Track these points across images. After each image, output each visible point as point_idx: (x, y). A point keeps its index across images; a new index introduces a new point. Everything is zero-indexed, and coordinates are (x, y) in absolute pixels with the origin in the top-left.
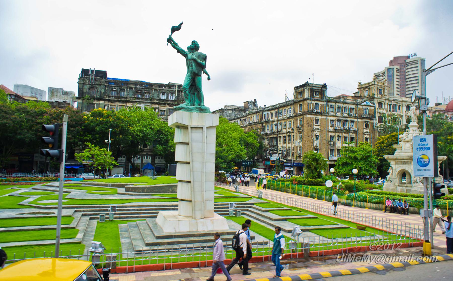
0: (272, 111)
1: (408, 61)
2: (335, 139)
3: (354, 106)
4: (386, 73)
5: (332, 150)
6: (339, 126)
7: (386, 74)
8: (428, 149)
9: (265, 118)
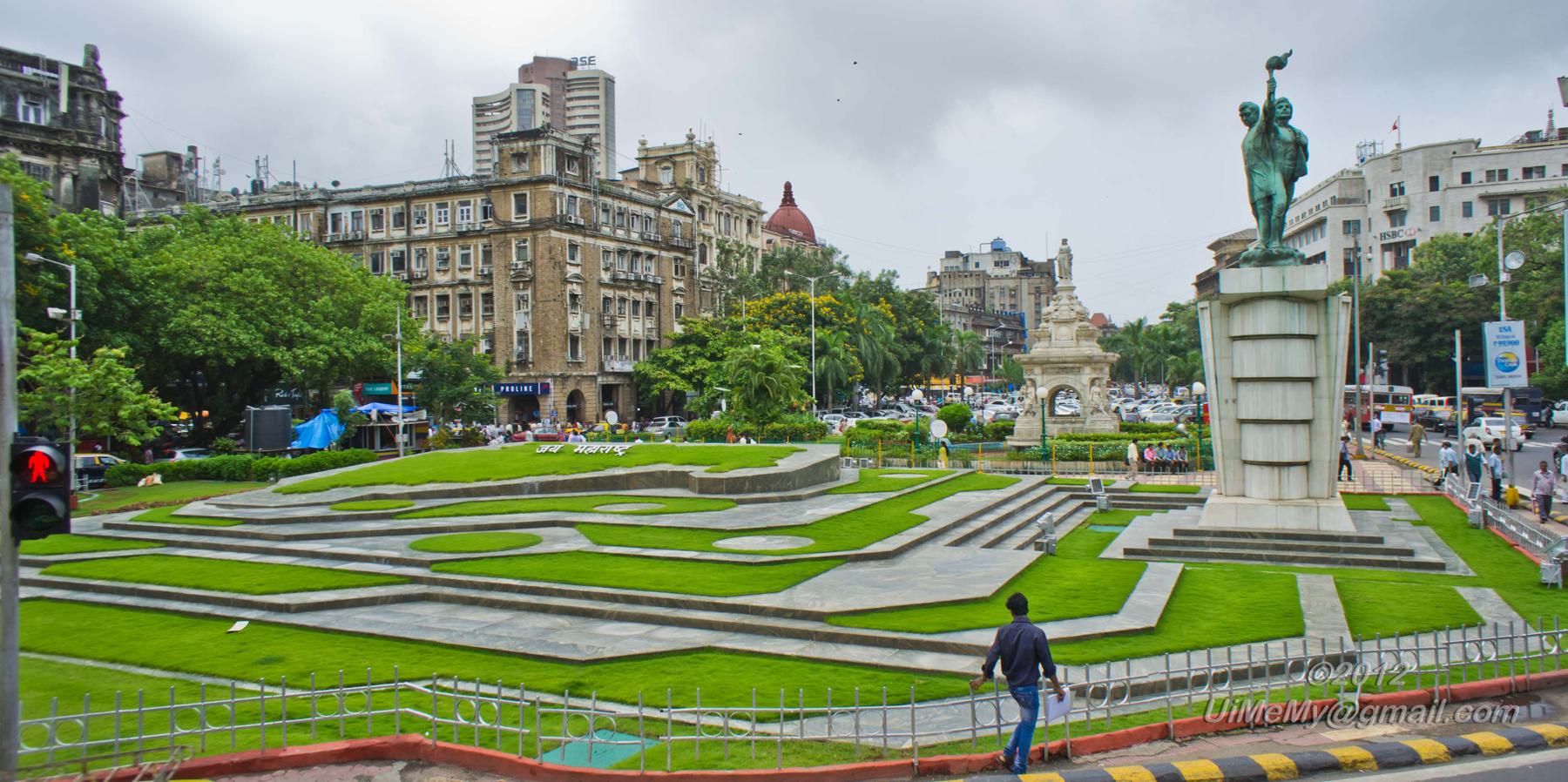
0: (376, 207)
1: (571, 75)
2: (614, 309)
3: (651, 212)
4: (514, 101)
5: (608, 341)
6: (622, 267)
7: (514, 107)
8: (1516, 343)
9: (335, 228)
